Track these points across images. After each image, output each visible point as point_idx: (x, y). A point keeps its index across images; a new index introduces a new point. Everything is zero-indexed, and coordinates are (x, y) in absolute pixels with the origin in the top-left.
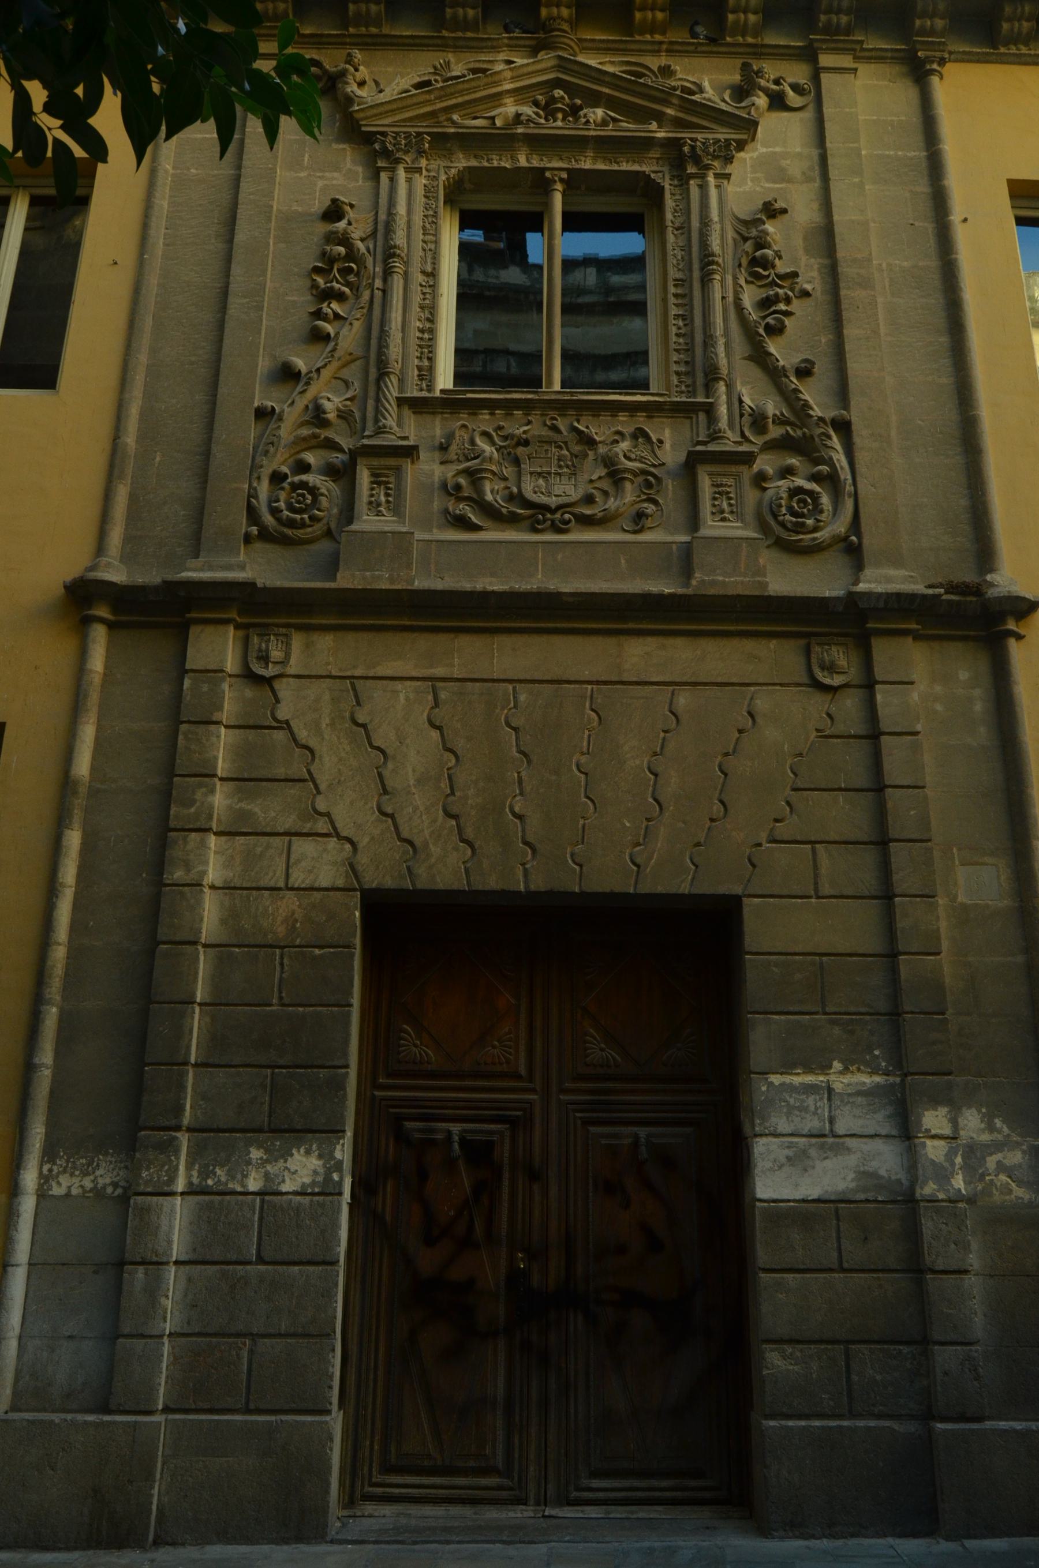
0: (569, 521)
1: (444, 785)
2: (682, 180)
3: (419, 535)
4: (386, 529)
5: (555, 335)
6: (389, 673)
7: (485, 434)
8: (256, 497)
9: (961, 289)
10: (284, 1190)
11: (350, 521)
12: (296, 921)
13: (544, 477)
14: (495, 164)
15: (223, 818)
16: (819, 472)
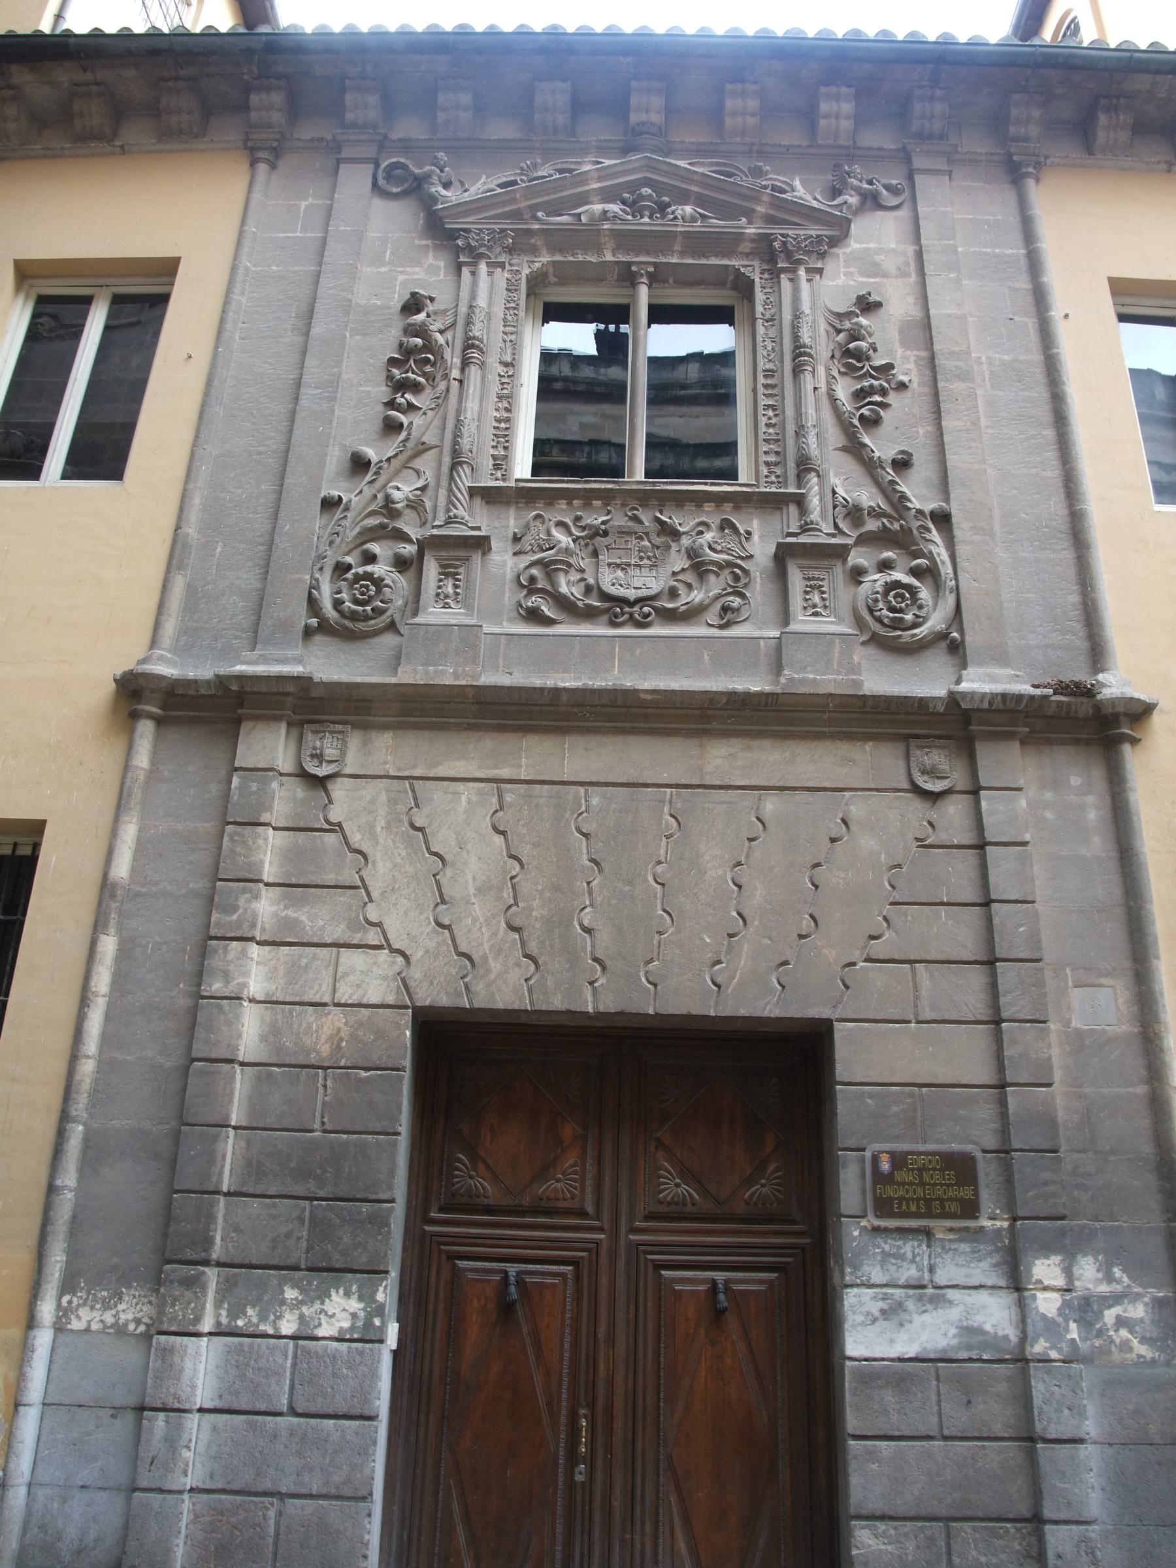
0: (649, 615)
1: (507, 895)
2: (774, 274)
3: (487, 628)
4: (453, 622)
5: (639, 424)
6: (451, 773)
7: (561, 524)
8: (318, 588)
9: (1064, 383)
10: (320, 1335)
11: (415, 613)
12: (341, 1039)
13: (623, 569)
14: (581, 258)
15: (267, 926)
16: (918, 566)
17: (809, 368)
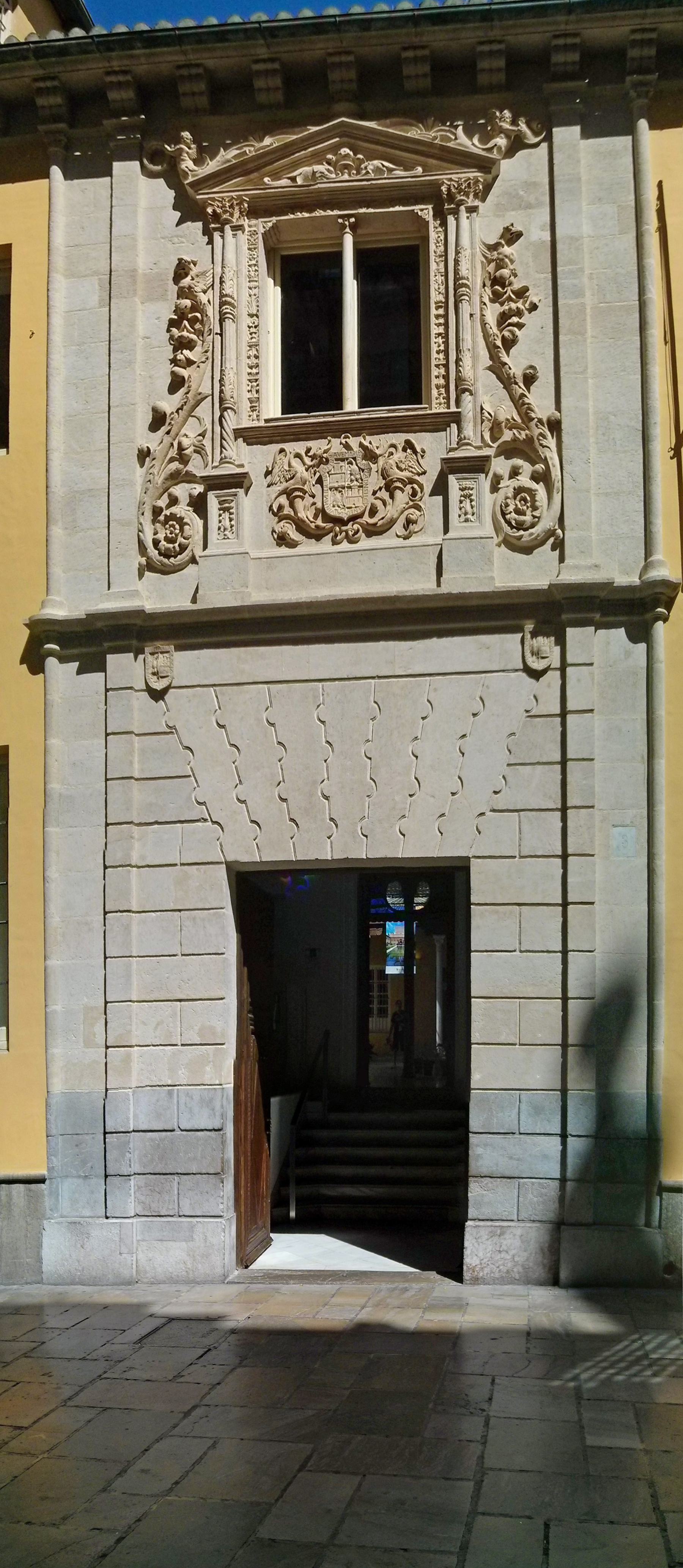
7: (298, 456)
13: (340, 492)
17: (467, 298)
